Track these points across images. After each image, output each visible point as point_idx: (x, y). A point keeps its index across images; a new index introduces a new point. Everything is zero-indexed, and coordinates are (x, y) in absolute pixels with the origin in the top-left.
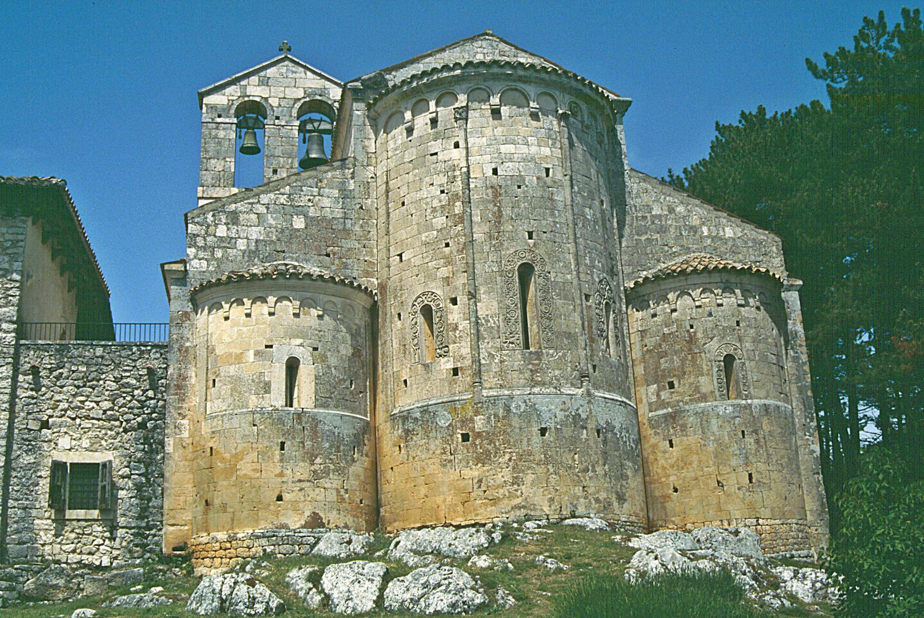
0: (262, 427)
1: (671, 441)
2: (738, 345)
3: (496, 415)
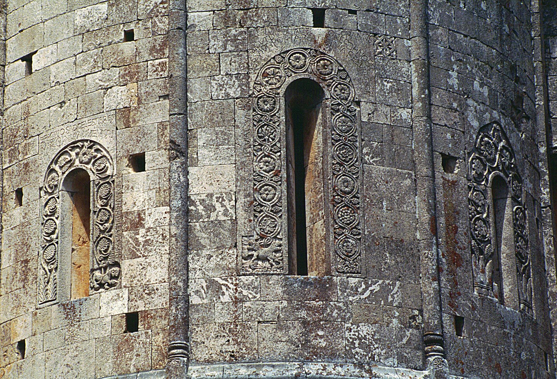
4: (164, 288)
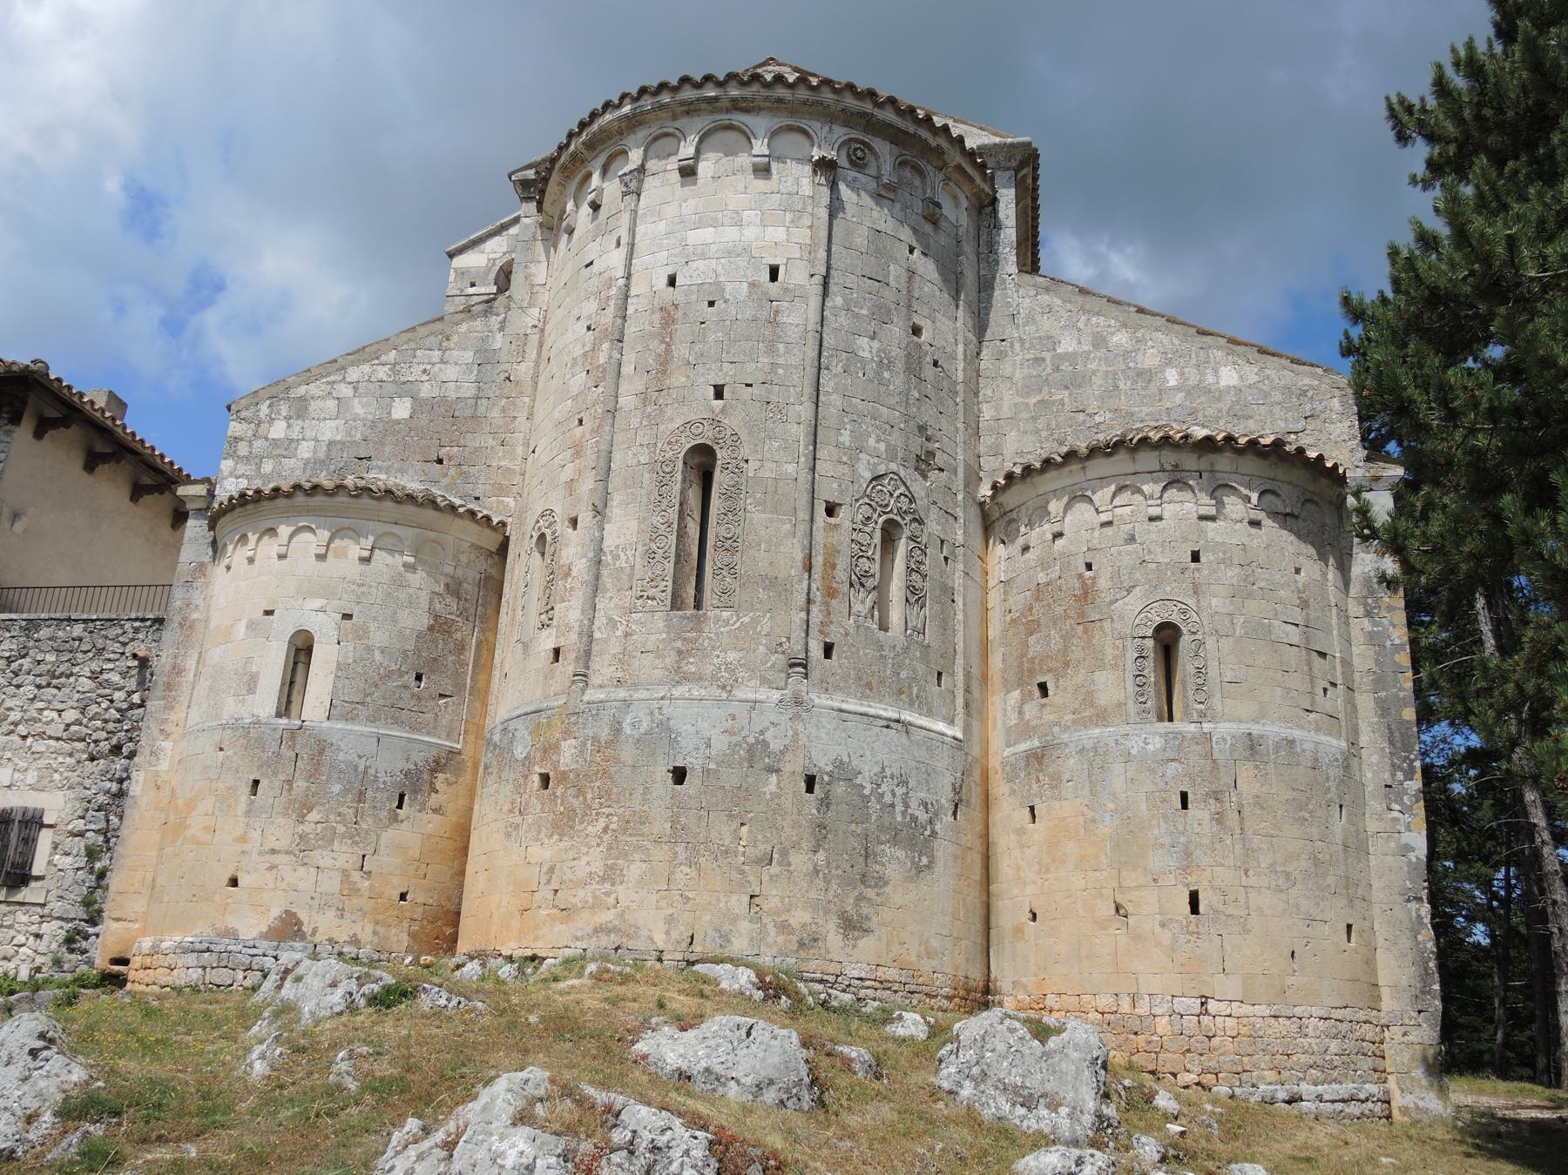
1: (1032, 809)
2: (1191, 602)
3: (595, 739)
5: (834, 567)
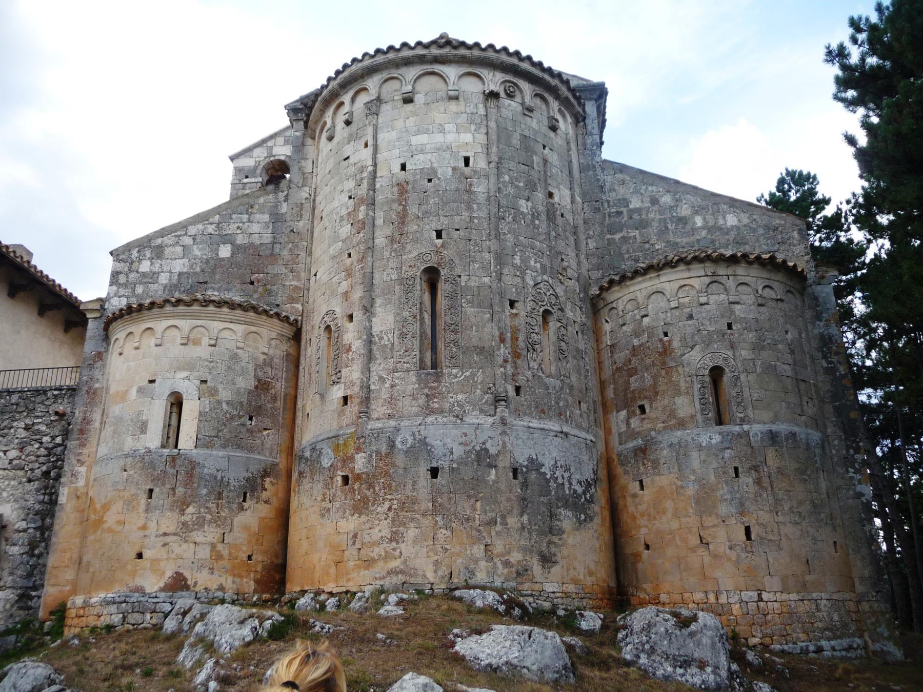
0: (132, 472)
1: (641, 482)
3: (378, 452)
4: (358, 382)
5: (517, 339)
